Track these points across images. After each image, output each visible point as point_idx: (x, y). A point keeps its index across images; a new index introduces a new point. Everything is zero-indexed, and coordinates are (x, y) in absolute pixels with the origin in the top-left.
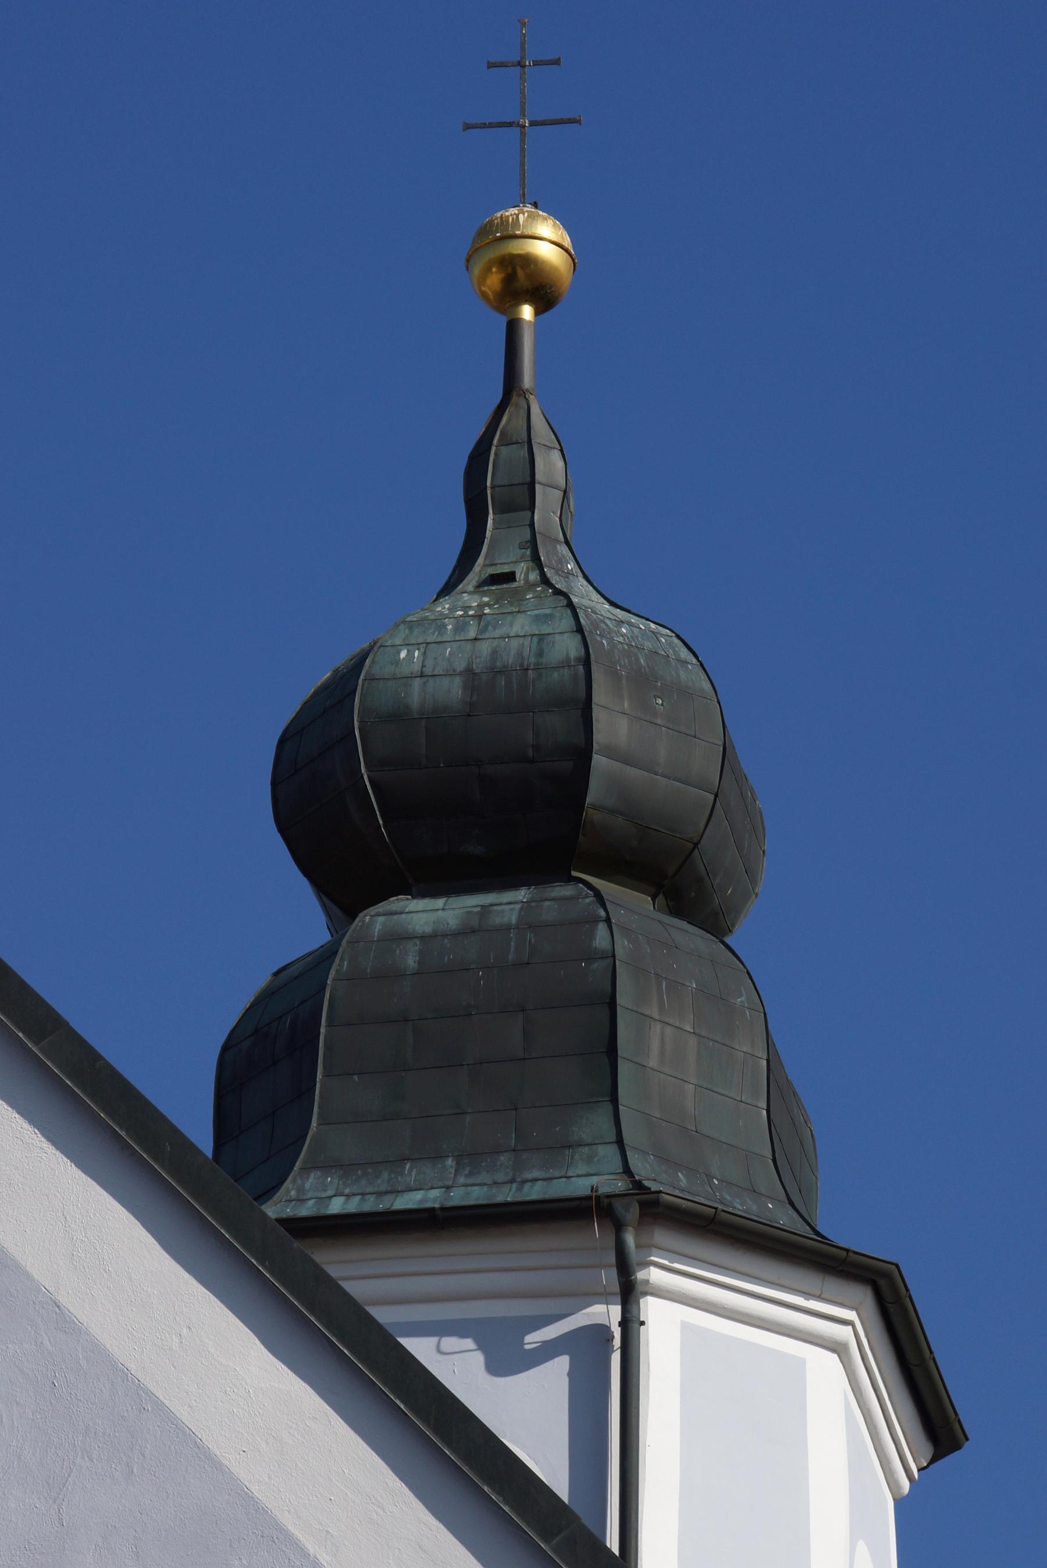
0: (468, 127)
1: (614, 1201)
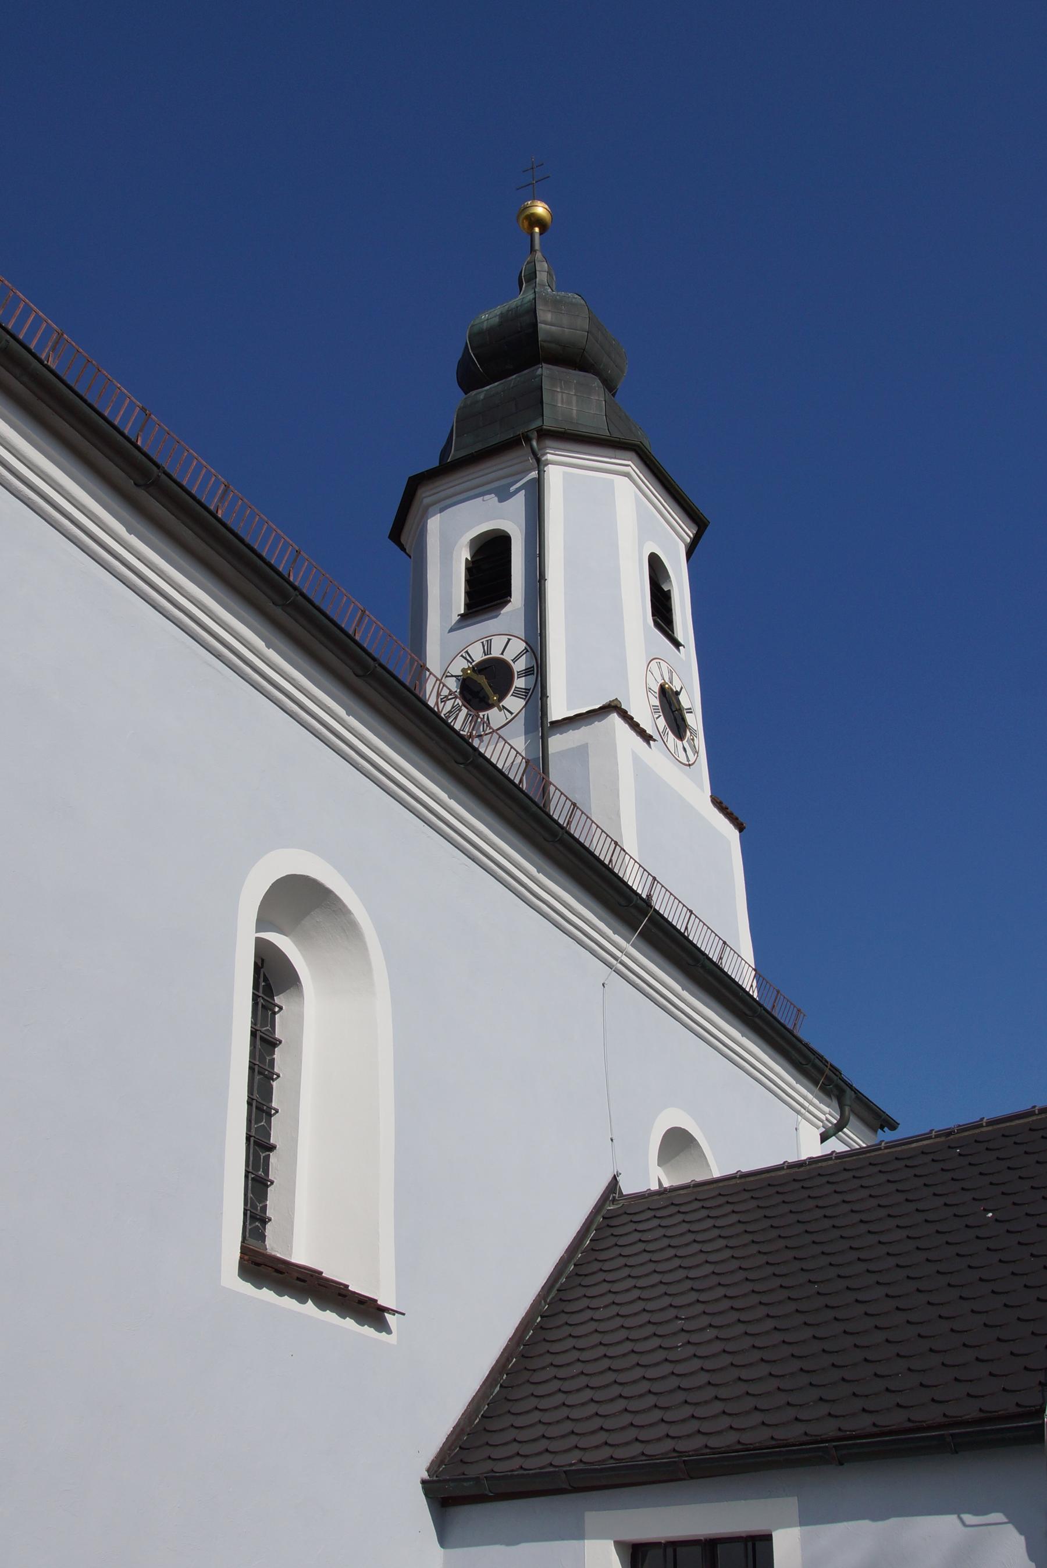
1: (529, 433)
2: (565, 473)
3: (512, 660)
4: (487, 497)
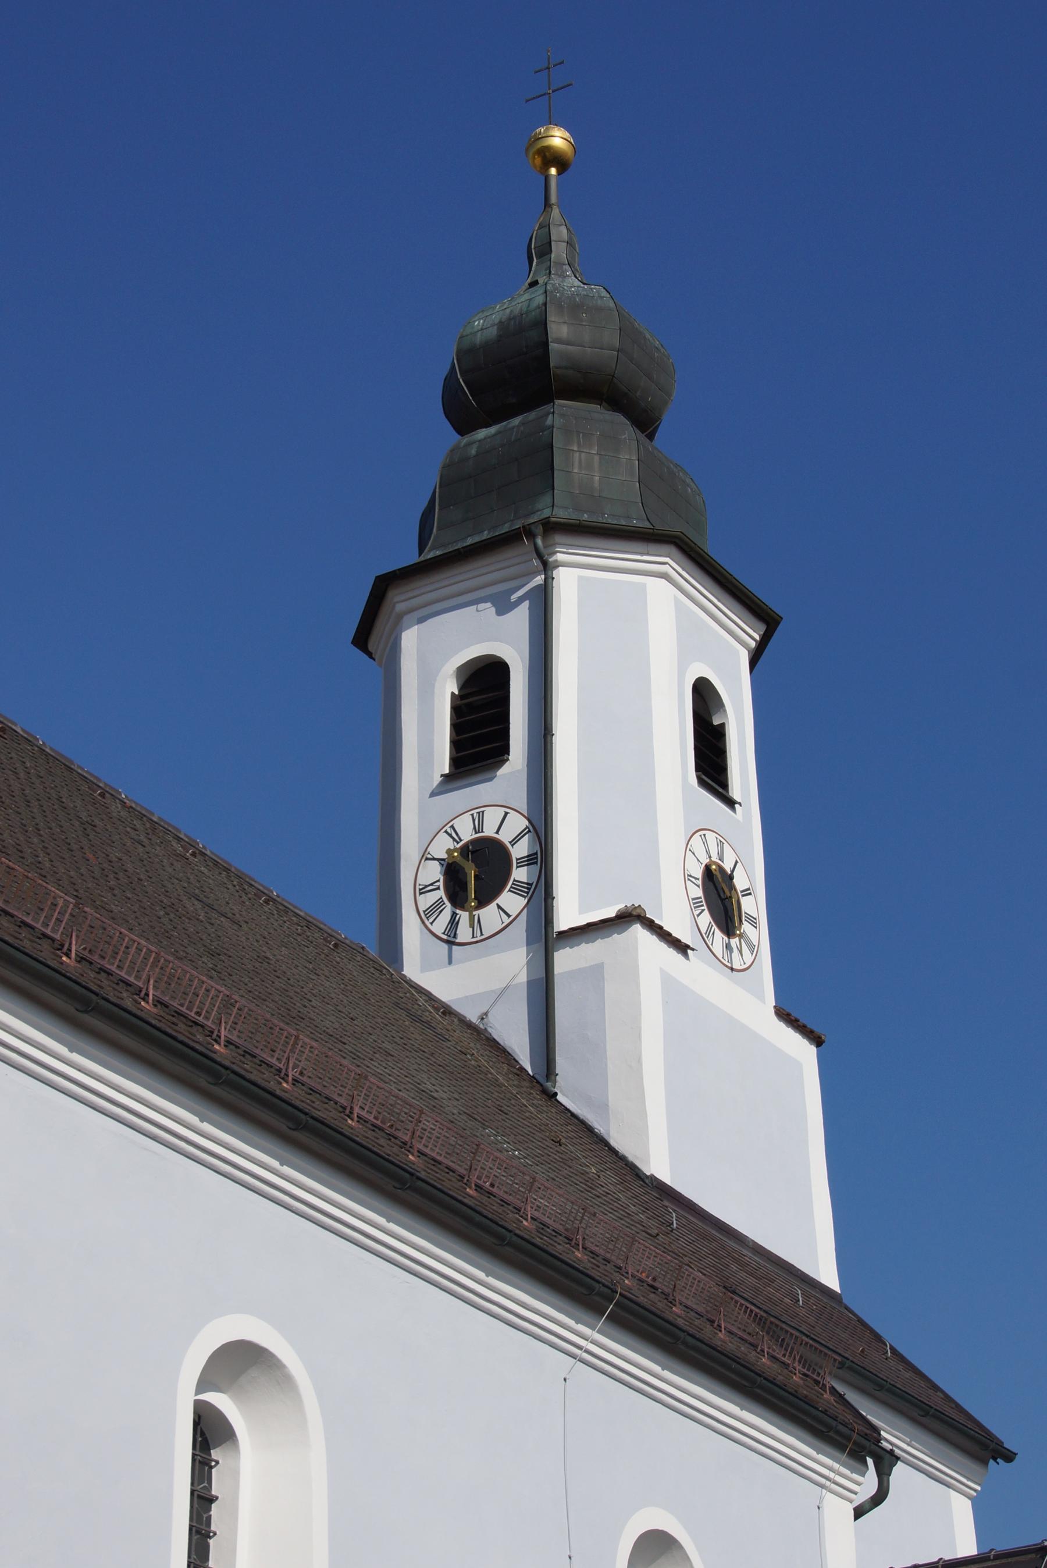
0: (527, 101)
2: (580, 578)
3: (510, 842)
4: (481, 606)
